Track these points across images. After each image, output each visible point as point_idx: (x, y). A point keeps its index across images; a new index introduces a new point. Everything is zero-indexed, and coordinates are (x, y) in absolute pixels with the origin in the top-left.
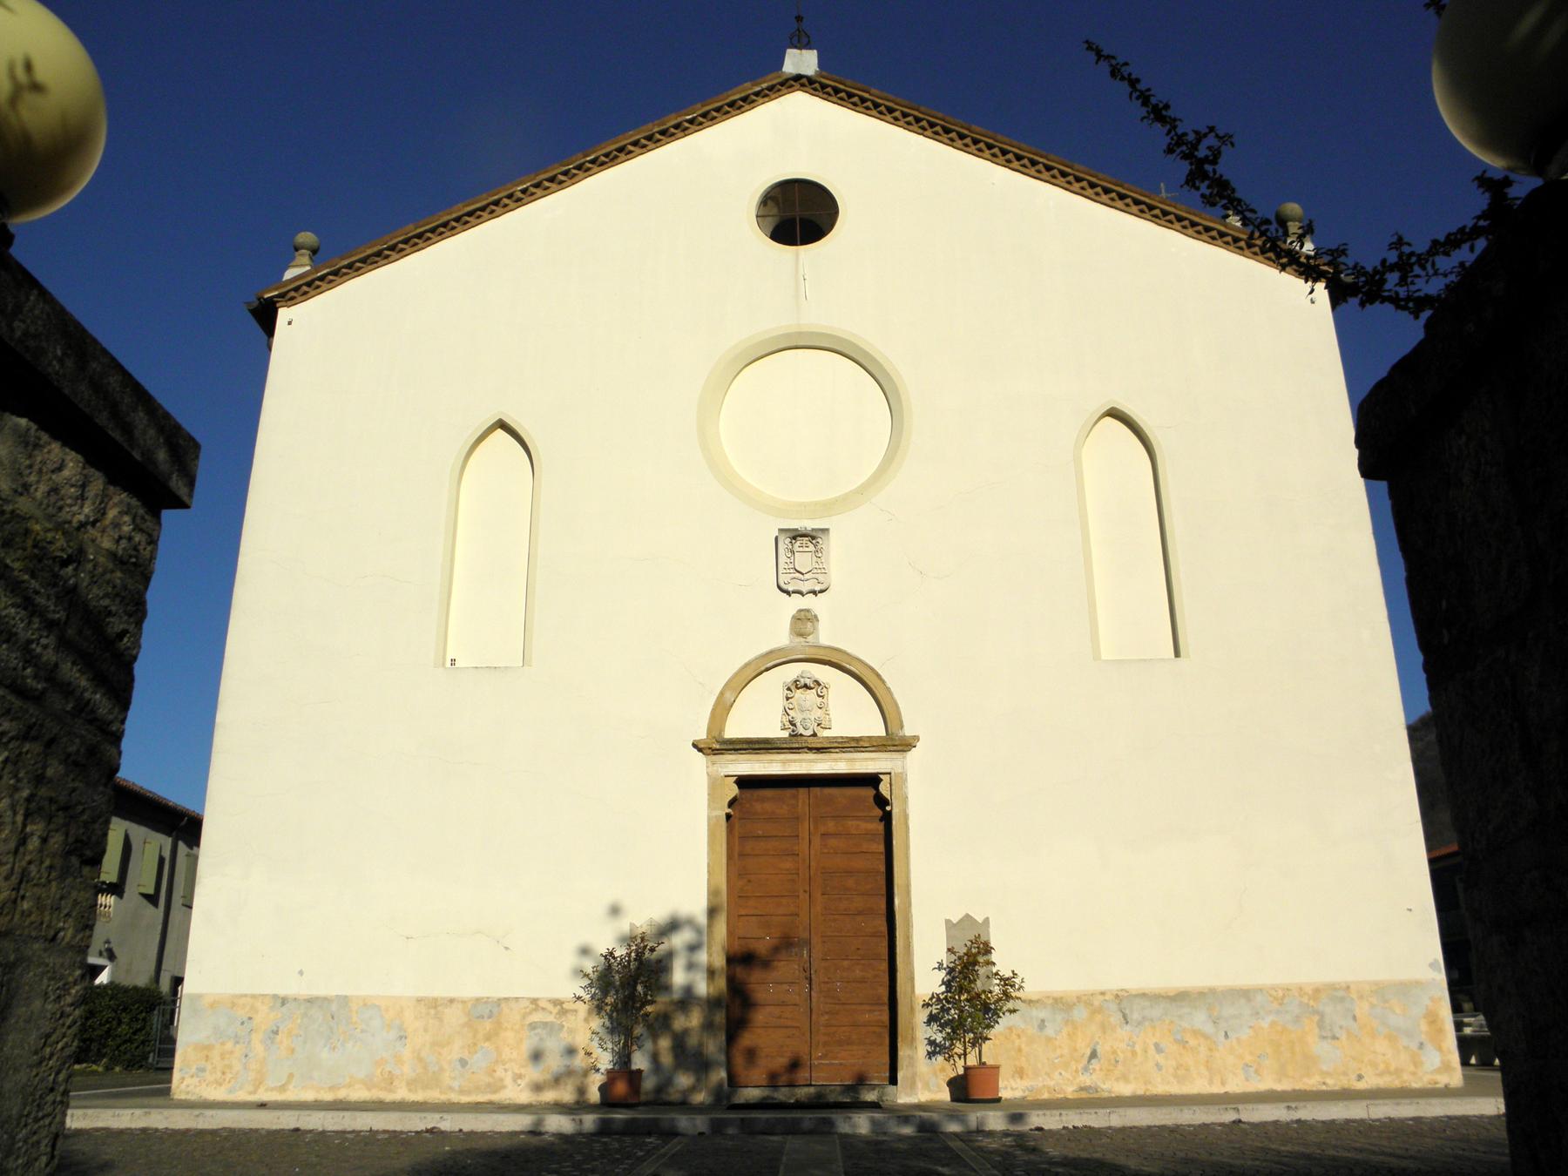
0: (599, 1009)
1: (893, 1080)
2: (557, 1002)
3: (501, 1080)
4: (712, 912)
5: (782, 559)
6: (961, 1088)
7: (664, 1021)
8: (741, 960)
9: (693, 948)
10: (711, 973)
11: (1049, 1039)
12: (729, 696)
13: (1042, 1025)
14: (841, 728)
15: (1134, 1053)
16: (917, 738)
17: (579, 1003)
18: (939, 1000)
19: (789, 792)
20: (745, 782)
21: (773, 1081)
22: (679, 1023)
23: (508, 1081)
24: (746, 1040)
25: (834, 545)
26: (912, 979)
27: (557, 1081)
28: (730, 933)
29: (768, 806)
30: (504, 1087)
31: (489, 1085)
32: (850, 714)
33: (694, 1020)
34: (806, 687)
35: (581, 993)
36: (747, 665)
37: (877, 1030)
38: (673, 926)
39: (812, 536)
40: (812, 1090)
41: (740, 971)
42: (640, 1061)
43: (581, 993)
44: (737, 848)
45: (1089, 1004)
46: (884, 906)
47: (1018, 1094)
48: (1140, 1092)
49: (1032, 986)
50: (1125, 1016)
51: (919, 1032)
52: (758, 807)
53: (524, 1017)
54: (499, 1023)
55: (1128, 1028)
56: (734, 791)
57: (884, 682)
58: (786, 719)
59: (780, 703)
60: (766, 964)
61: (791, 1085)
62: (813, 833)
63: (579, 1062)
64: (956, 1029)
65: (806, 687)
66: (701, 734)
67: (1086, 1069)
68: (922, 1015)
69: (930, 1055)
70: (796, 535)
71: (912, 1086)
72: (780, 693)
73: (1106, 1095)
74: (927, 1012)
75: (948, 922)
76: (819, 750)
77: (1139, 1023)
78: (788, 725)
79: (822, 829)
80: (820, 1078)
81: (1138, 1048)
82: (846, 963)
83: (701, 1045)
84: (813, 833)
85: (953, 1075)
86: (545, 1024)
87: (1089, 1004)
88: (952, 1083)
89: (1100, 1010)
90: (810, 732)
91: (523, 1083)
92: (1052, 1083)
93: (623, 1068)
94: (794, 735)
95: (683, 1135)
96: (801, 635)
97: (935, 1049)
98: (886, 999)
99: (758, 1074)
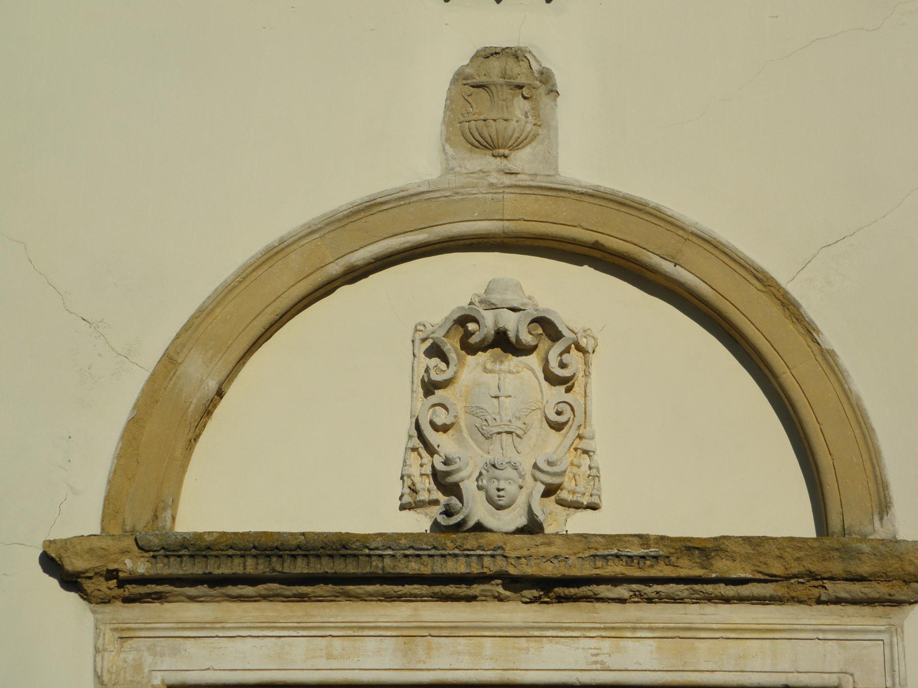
12: (199, 374)
34: (503, 342)
36: (274, 254)
57: (809, 330)
58: (420, 467)
59: (401, 404)
65: (503, 342)
66: (80, 517)
72: (403, 367)
76: (550, 588)
78: (427, 489)
90: (514, 519)
94: (453, 527)
95: (491, 531)
96: (487, 145)
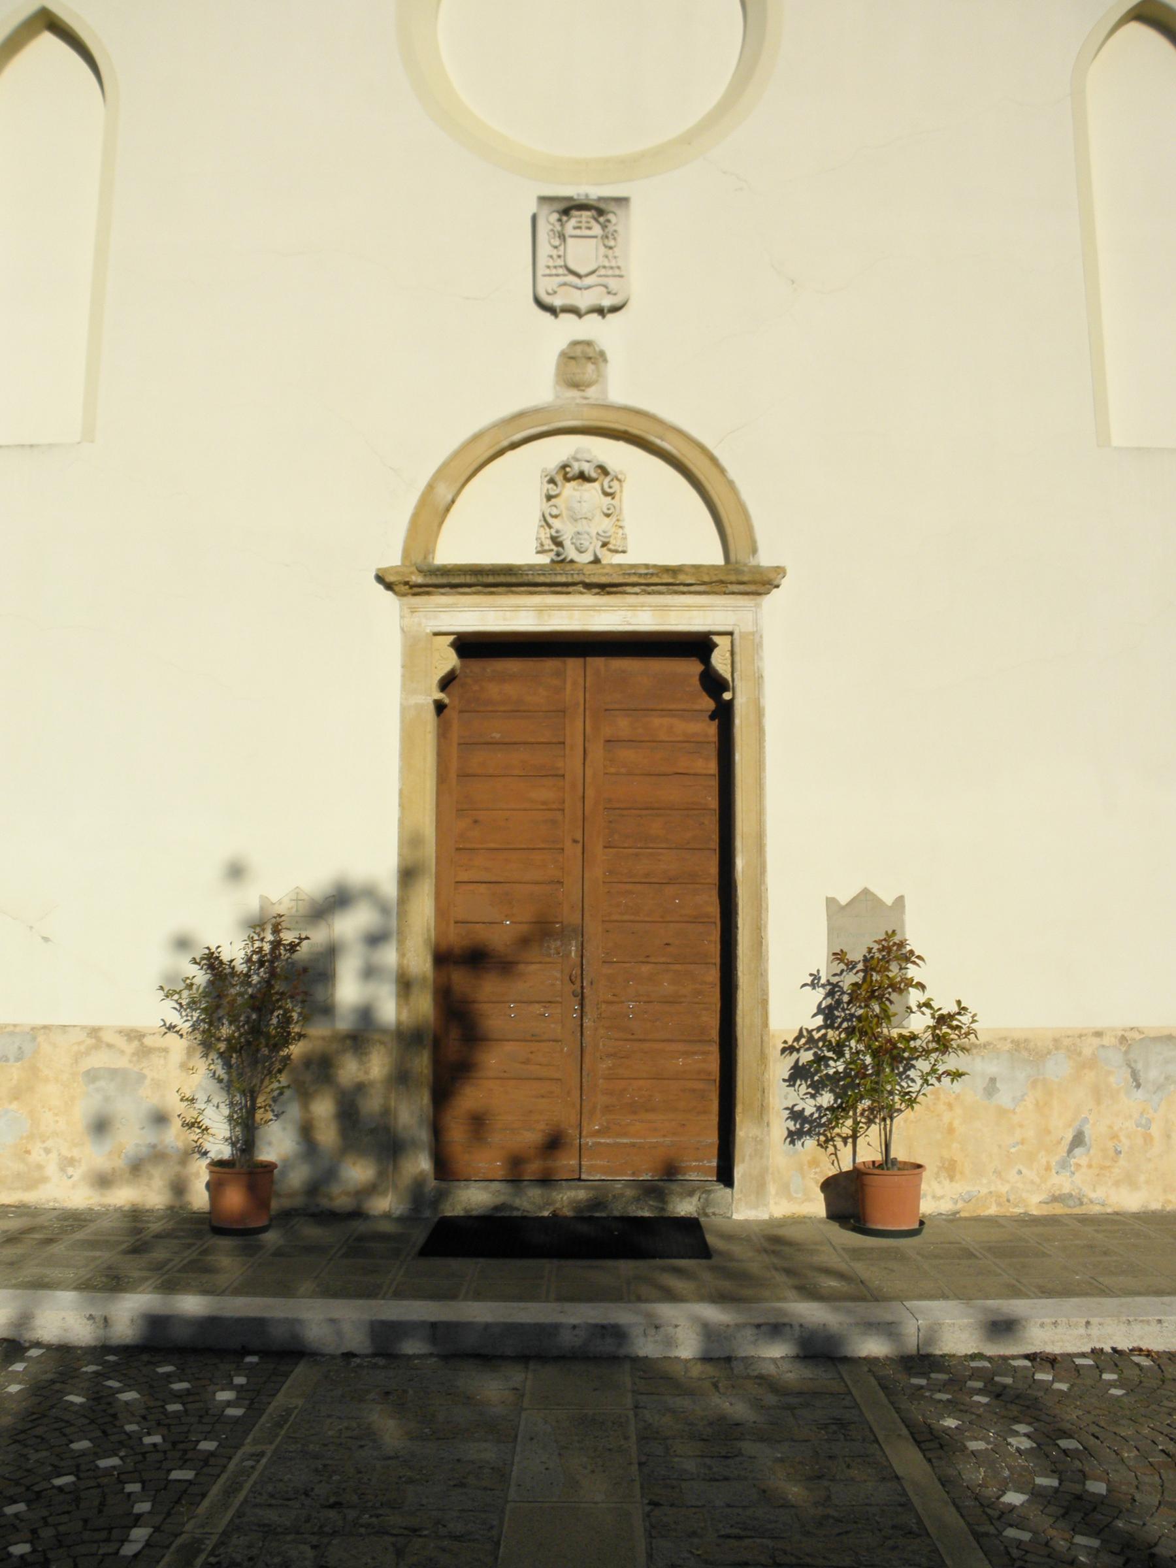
0: (207, 1045)
1: (726, 1176)
2: (134, 1035)
3: (40, 1167)
4: (408, 875)
5: (544, 249)
6: (849, 1198)
7: (321, 1068)
8: (462, 962)
9: (375, 939)
10: (405, 985)
11: (1002, 1112)
12: (444, 492)
13: (991, 1086)
14: (644, 548)
15: (1148, 1139)
16: (780, 571)
17: (172, 1037)
18: (811, 1041)
19: (550, 665)
20: (472, 647)
21: (515, 1176)
22: (349, 1070)
23: (52, 1169)
24: (469, 1098)
25: (638, 228)
26: (764, 1003)
27: (137, 1168)
28: (442, 912)
29: (511, 690)
30: (44, 1180)
31: (18, 1176)
32: (659, 523)
33: (376, 1066)
34: (583, 477)
35: (174, 1018)
36: (476, 438)
37: (700, 1085)
38: (339, 899)
39: (598, 209)
40: (581, 1195)
41: (459, 978)
42: (277, 1144)
43: (174, 1018)
44: (454, 765)
45: (1073, 1052)
46: (714, 869)
47: (945, 1207)
48: (1155, 1206)
49: (990, 1018)
50: (1135, 1075)
51: (773, 1095)
52: (494, 690)
53: (77, 1058)
54: (34, 1070)
55: (1139, 1094)
56: (449, 660)
57: (722, 471)
58: (545, 535)
59: (536, 505)
60: (506, 966)
61: (546, 1181)
62: (592, 728)
63: (174, 1137)
64: (848, 1090)
66: (392, 558)
67: (1063, 1165)
68: (781, 1067)
69: (793, 1137)
70: (569, 208)
71: (760, 1188)
72: (536, 488)
73: (1096, 1209)
74: (790, 1060)
75: (831, 902)
76: (604, 588)
77: (1160, 1088)
78: (548, 544)
79: (607, 731)
80: (596, 1169)
81: (1155, 1130)
82: (645, 969)
83: (386, 1112)
84: (592, 728)
85: (832, 1171)
86: (113, 1073)
87: (1073, 1052)
88: (829, 1186)
89: (1092, 1063)
90: (587, 557)
91: (77, 1172)
92: (1004, 1189)
93: (243, 1167)
96: (576, 385)
97: (802, 1126)
98: (715, 1034)
99: (487, 1160)
